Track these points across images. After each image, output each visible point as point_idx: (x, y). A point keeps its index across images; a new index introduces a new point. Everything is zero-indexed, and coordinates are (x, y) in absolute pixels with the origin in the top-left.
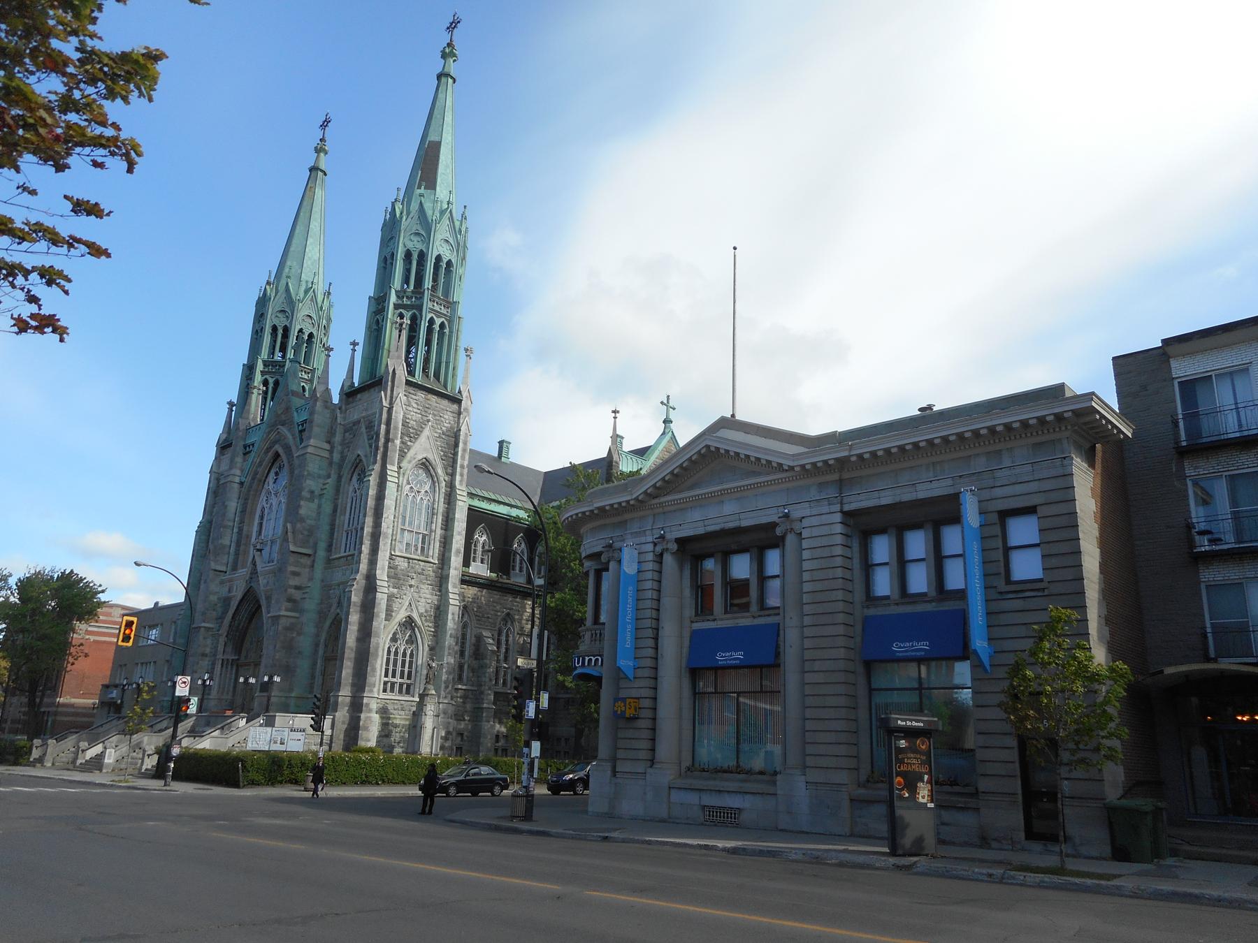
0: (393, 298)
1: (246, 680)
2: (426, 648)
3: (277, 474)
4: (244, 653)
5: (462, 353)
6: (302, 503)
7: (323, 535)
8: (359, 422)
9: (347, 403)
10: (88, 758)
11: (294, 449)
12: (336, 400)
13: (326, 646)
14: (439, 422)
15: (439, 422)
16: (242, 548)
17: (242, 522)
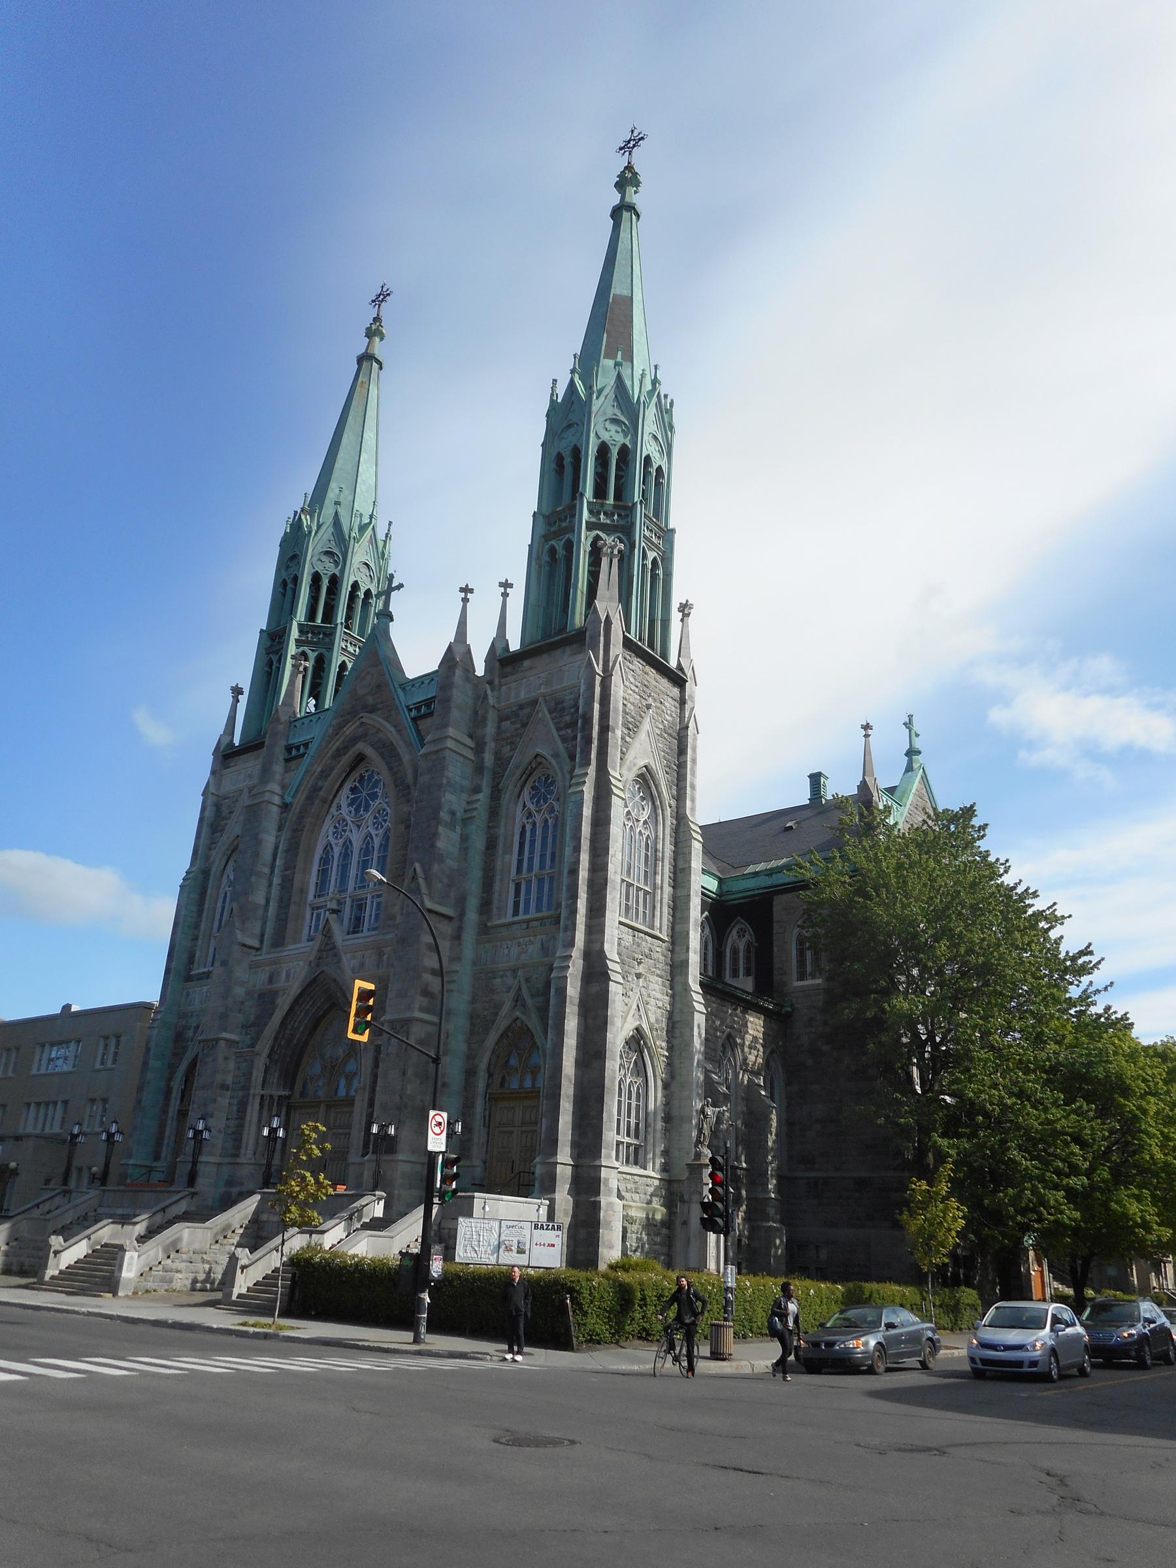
0: (295, 633)
1: (382, 1128)
2: (660, 1083)
3: (353, 790)
4: (298, 1087)
5: (676, 616)
6: (441, 829)
7: (474, 887)
8: (534, 702)
9: (503, 676)
10: (63, 1267)
11: (402, 749)
12: (480, 670)
13: (490, 1075)
14: (660, 712)
15: (660, 712)
16: (293, 909)
17: (289, 867)
